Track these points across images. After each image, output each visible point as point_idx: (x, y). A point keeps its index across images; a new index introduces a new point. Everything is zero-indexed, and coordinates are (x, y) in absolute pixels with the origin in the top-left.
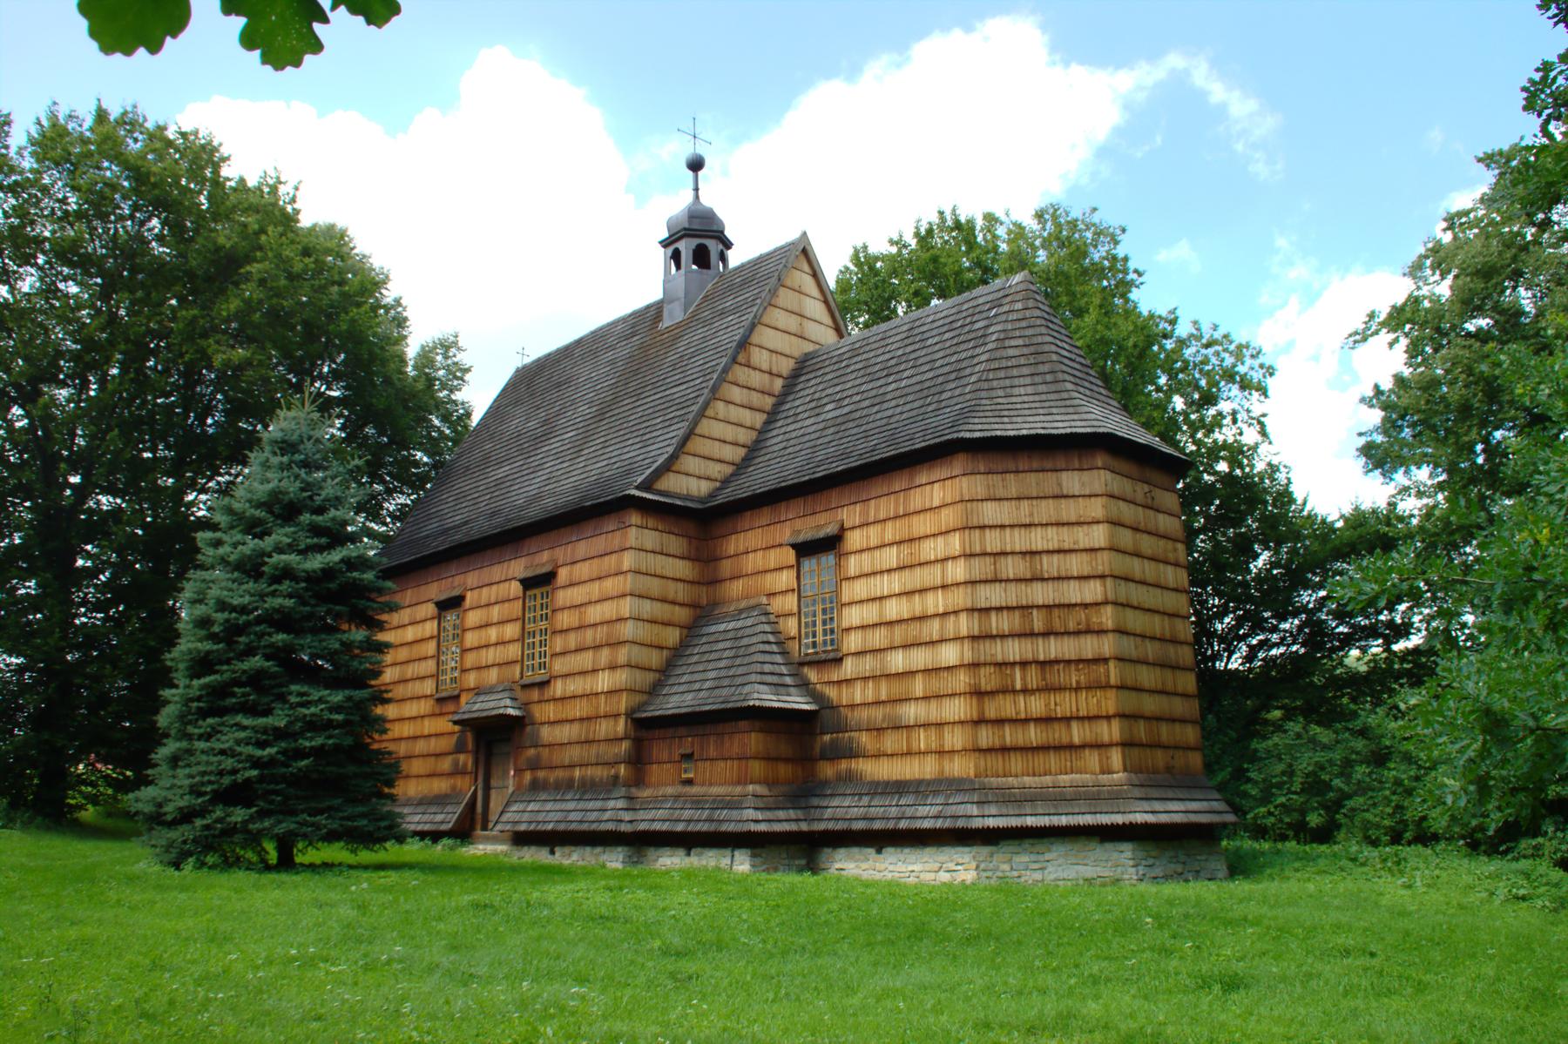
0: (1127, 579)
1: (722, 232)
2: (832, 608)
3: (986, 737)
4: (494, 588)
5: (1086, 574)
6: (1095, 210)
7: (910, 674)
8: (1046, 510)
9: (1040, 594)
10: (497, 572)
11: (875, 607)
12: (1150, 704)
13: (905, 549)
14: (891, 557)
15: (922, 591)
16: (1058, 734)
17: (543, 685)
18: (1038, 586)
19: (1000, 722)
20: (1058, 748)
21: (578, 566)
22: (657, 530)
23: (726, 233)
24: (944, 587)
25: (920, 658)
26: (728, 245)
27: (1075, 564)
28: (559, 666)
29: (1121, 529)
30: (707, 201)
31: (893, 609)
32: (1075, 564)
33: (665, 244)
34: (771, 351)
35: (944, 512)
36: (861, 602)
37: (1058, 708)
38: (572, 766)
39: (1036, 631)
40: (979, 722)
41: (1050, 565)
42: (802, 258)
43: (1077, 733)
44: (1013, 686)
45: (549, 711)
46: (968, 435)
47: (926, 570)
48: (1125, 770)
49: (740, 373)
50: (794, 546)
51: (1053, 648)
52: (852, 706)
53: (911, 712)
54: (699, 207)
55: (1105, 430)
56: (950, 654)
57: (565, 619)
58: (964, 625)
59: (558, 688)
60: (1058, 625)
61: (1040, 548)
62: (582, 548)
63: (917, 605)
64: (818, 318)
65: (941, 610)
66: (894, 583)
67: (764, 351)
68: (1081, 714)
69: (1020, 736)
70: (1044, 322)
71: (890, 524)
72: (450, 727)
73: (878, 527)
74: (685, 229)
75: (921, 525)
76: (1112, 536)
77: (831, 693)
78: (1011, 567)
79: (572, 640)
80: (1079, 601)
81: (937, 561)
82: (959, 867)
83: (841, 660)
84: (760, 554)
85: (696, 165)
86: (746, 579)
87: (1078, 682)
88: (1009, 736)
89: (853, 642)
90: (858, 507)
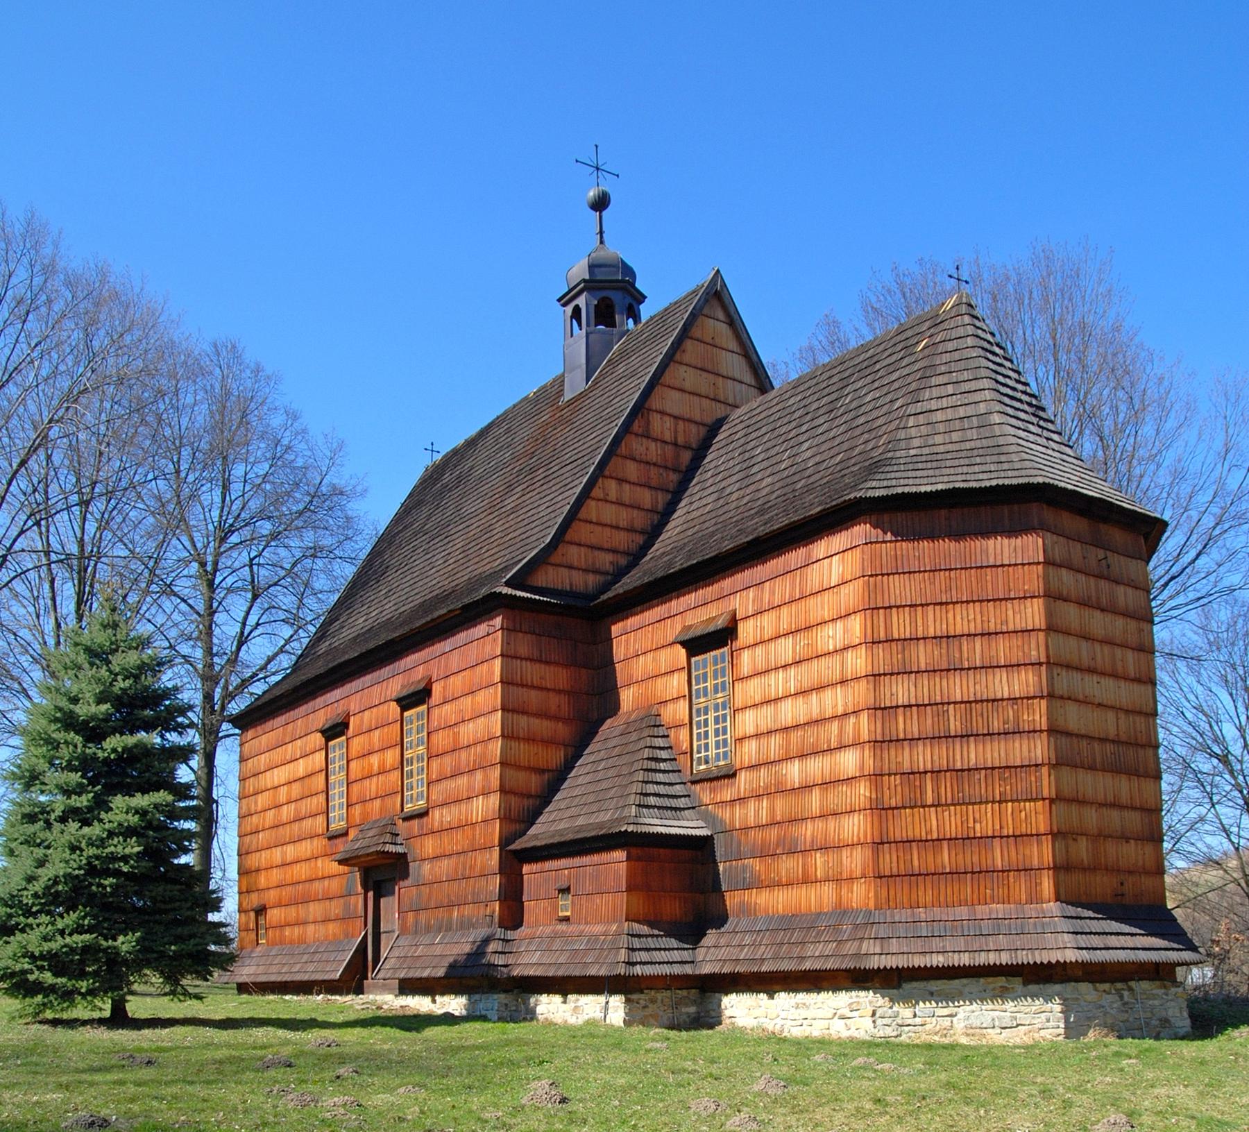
0: (1068, 667)
1: (633, 285)
2: (724, 716)
3: (889, 861)
4: (374, 710)
7: (807, 787)
8: (965, 584)
9: (958, 688)
10: (376, 694)
11: (768, 710)
12: (1091, 818)
13: (802, 639)
14: (785, 649)
15: (820, 688)
17: (423, 814)
18: (956, 678)
20: (671, 808)
21: (452, 679)
22: (534, 633)
23: (637, 285)
24: (842, 682)
25: (817, 767)
26: (641, 298)
27: (1002, 650)
31: (790, 712)
32: (1002, 650)
33: (564, 300)
34: (675, 417)
35: (844, 590)
37: (978, 826)
42: (715, 303)
43: (998, 856)
45: (429, 846)
46: (870, 494)
47: (824, 661)
48: (1058, 899)
49: (637, 446)
50: (684, 644)
51: (972, 754)
52: (745, 829)
53: (808, 831)
55: (1041, 480)
56: (849, 762)
62: (456, 660)
63: (814, 705)
64: (737, 376)
65: (840, 711)
67: (667, 418)
69: (930, 859)
70: (982, 353)
71: (785, 610)
72: (335, 867)
73: (773, 614)
74: (584, 281)
76: (1049, 614)
77: (725, 814)
78: (922, 656)
82: (854, 1014)
83: (734, 775)
84: (650, 655)
85: (601, 204)
89: (749, 752)
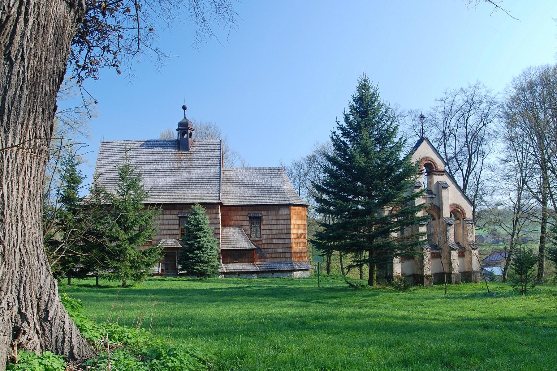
31: (274, 232)
52: (265, 249)
66: (275, 227)
89: (264, 237)
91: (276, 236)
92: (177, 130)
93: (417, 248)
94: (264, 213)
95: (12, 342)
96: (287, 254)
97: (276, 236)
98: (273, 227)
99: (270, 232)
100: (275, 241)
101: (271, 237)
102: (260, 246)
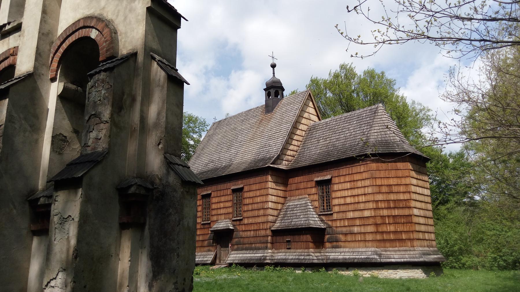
5: (405, 191)
6: (359, 37)
8: (393, 173)
9: (392, 197)
16: (399, 236)
19: (382, 233)
28: (245, 215)
29: (413, 179)
30: (278, 76)
31: (348, 200)
35: (364, 174)
36: (338, 198)
38: (372, 241)
39: (392, 207)
40: (377, 232)
41: (395, 189)
44: (386, 222)
51: (396, 212)
52: (337, 227)
53: (356, 229)
54: (275, 79)
57: (247, 201)
58: (371, 205)
59: (246, 221)
60: (397, 205)
61: (392, 184)
66: (349, 193)
68: (405, 230)
71: (347, 176)
75: (357, 177)
79: (250, 207)
80: (403, 199)
81: (362, 187)
85: (273, 66)
86: (301, 190)
87: (404, 221)
88: (385, 237)
89: (336, 209)
90: (337, 171)
91: (351, 207)
92: (265, 90)
93: (60, 222)
94: (335, 172)
95: (132, 186)
96: (367, 236)
97: (351, 207)
98: (346, 193)
99: (342, 201)
100: (351, 215)
101: (343, 208)
102: (330, 223)
